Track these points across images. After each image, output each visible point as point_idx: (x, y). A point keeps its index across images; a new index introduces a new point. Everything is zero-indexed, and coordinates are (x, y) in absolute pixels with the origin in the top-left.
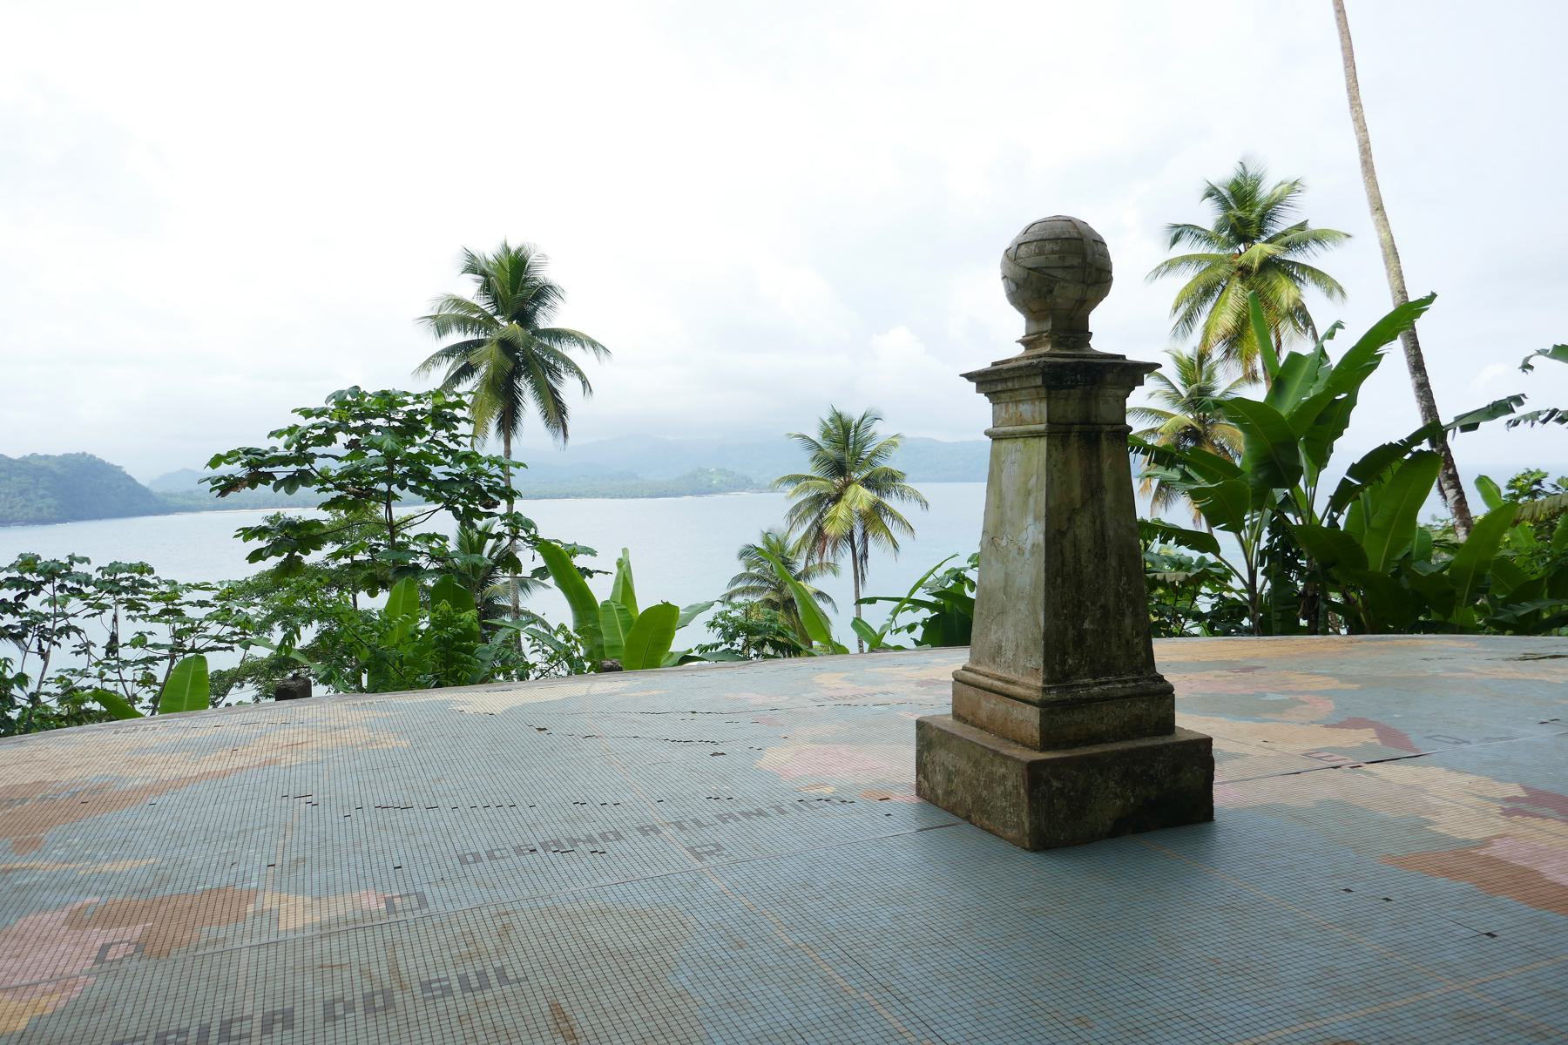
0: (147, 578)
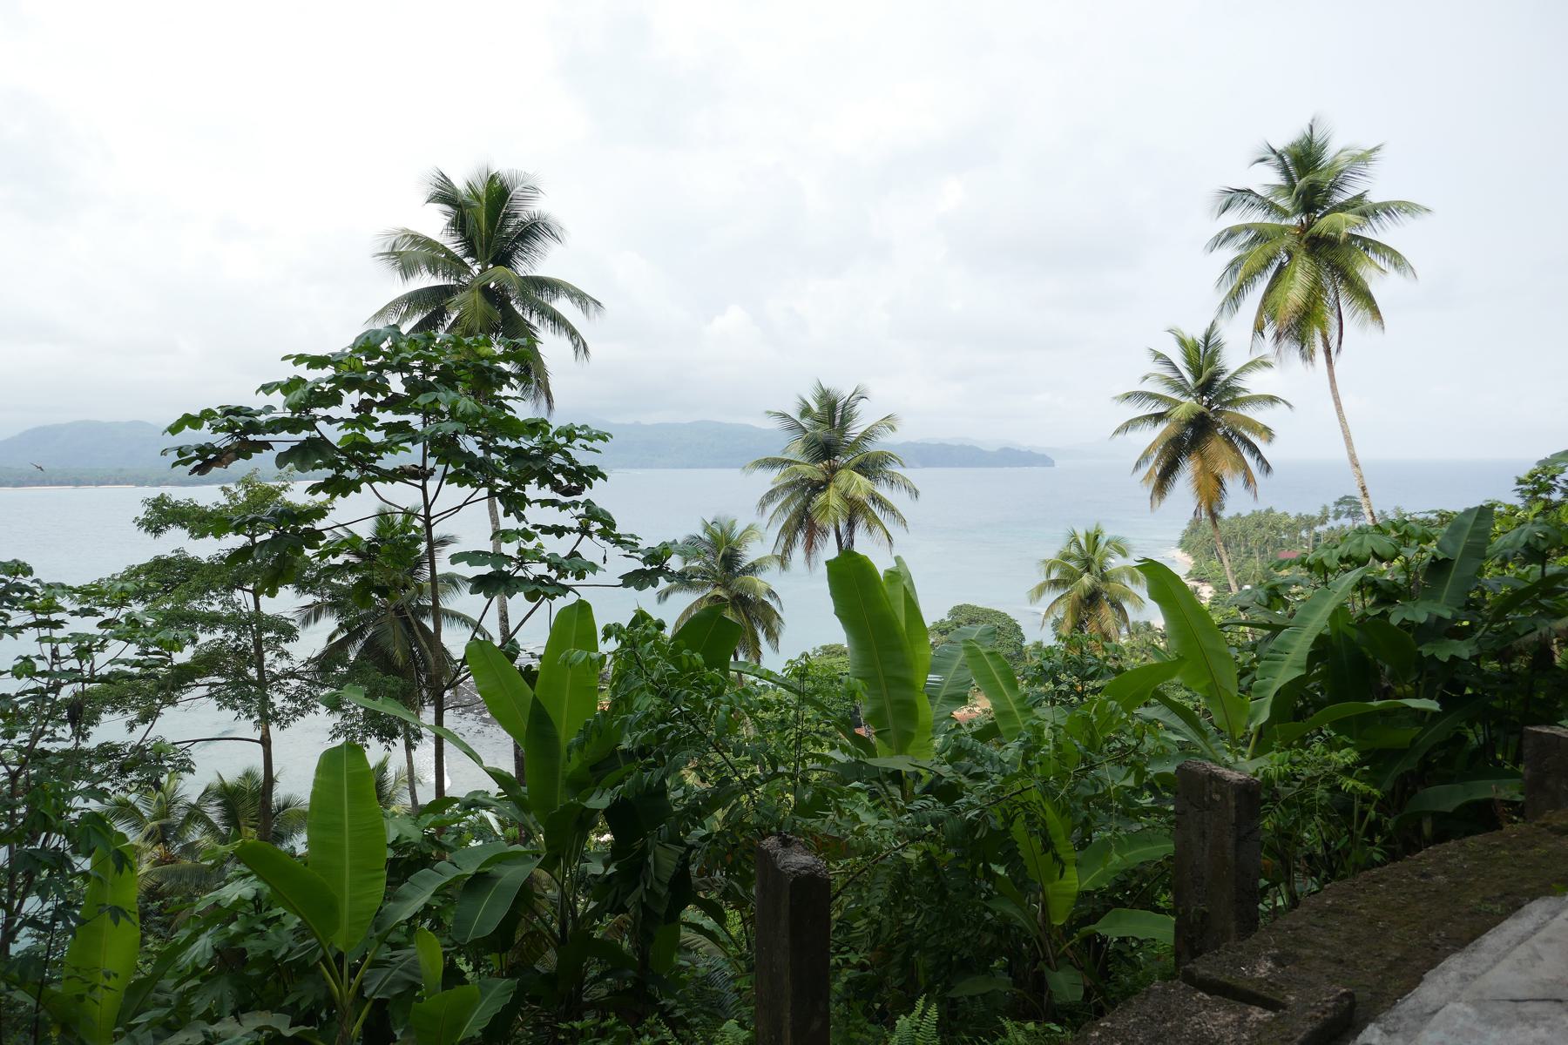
0: (26, 581)
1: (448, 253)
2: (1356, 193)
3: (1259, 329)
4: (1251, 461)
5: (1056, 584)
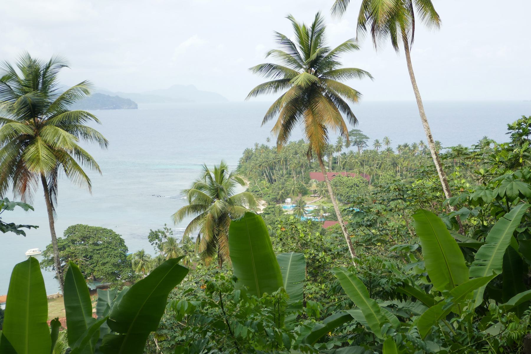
3: (362, 23)
4: (344, 116)
5: (194, 208)
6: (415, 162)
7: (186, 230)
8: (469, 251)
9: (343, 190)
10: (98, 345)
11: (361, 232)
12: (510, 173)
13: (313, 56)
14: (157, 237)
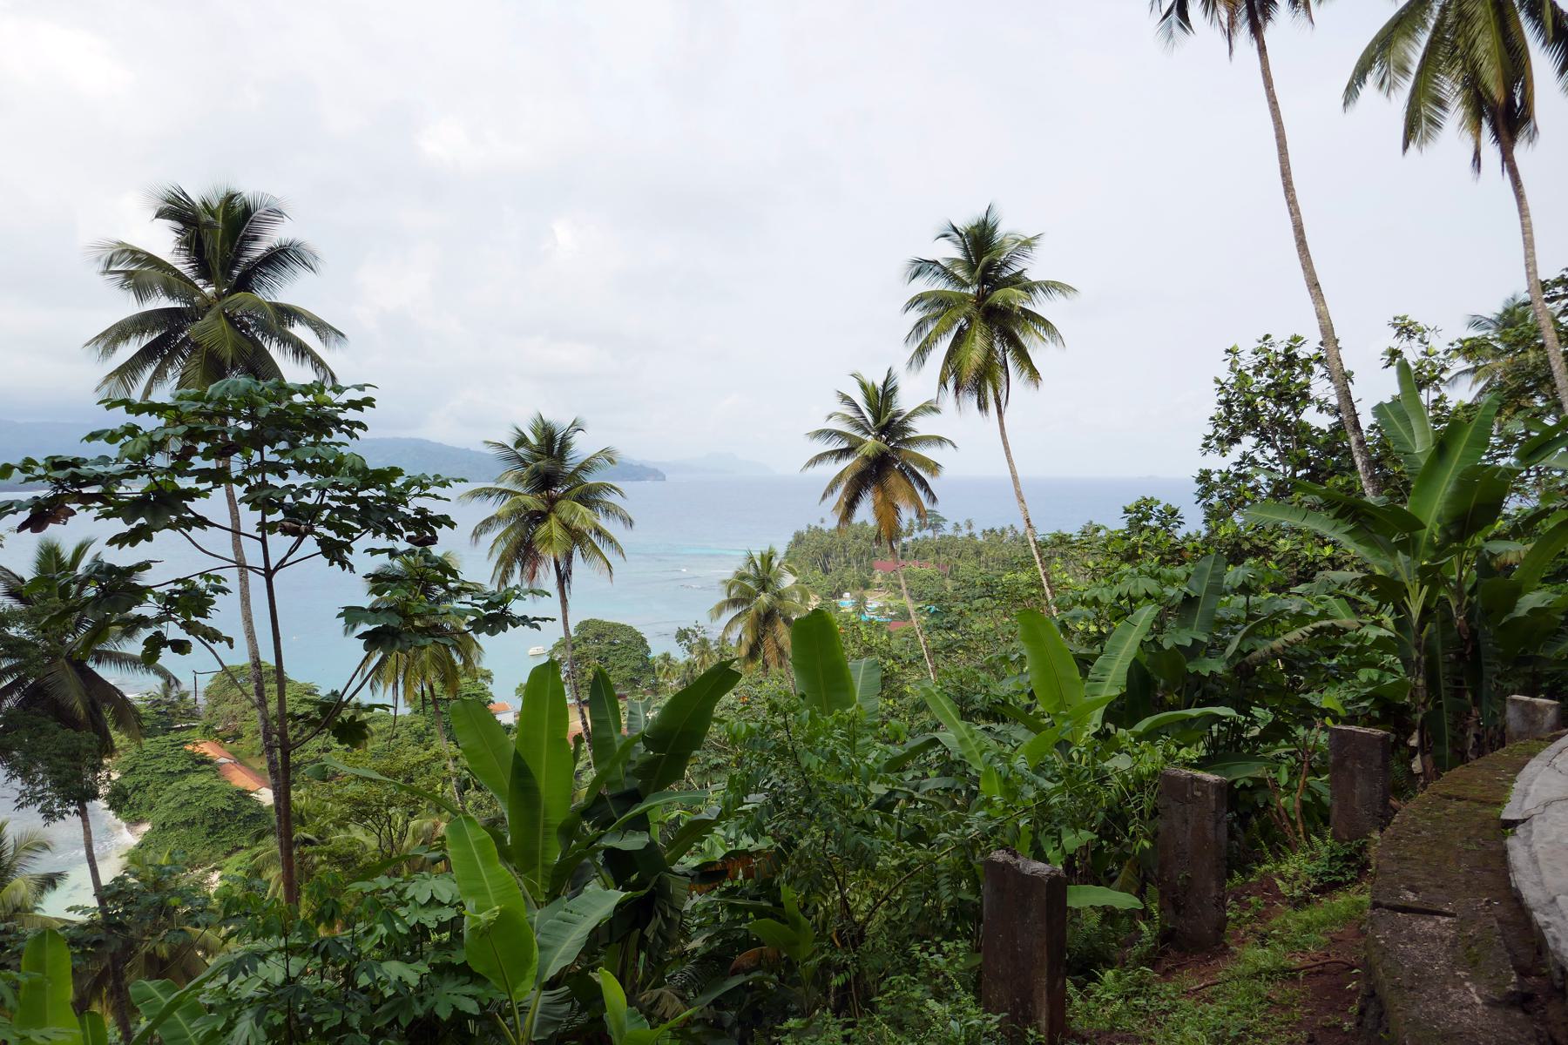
1: (178, 274)
2: (1017, 269)
3: (943, 382)
4: (921, 493)
5: (734, 603)
6: (1007, 551)
7: (726, 631)
8: (1084, 663)
9: (915, 584)
10: (630, 768)
11: (939, 638)
12: (1126, 567)
13: (884, 421)
14: (686, 637)
